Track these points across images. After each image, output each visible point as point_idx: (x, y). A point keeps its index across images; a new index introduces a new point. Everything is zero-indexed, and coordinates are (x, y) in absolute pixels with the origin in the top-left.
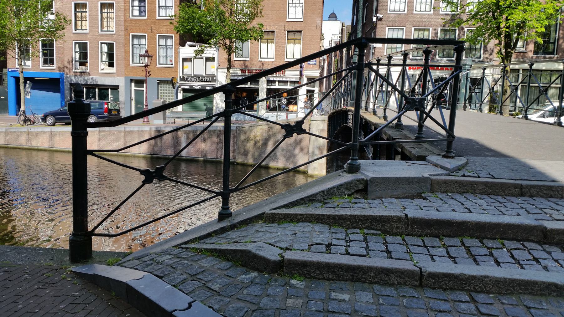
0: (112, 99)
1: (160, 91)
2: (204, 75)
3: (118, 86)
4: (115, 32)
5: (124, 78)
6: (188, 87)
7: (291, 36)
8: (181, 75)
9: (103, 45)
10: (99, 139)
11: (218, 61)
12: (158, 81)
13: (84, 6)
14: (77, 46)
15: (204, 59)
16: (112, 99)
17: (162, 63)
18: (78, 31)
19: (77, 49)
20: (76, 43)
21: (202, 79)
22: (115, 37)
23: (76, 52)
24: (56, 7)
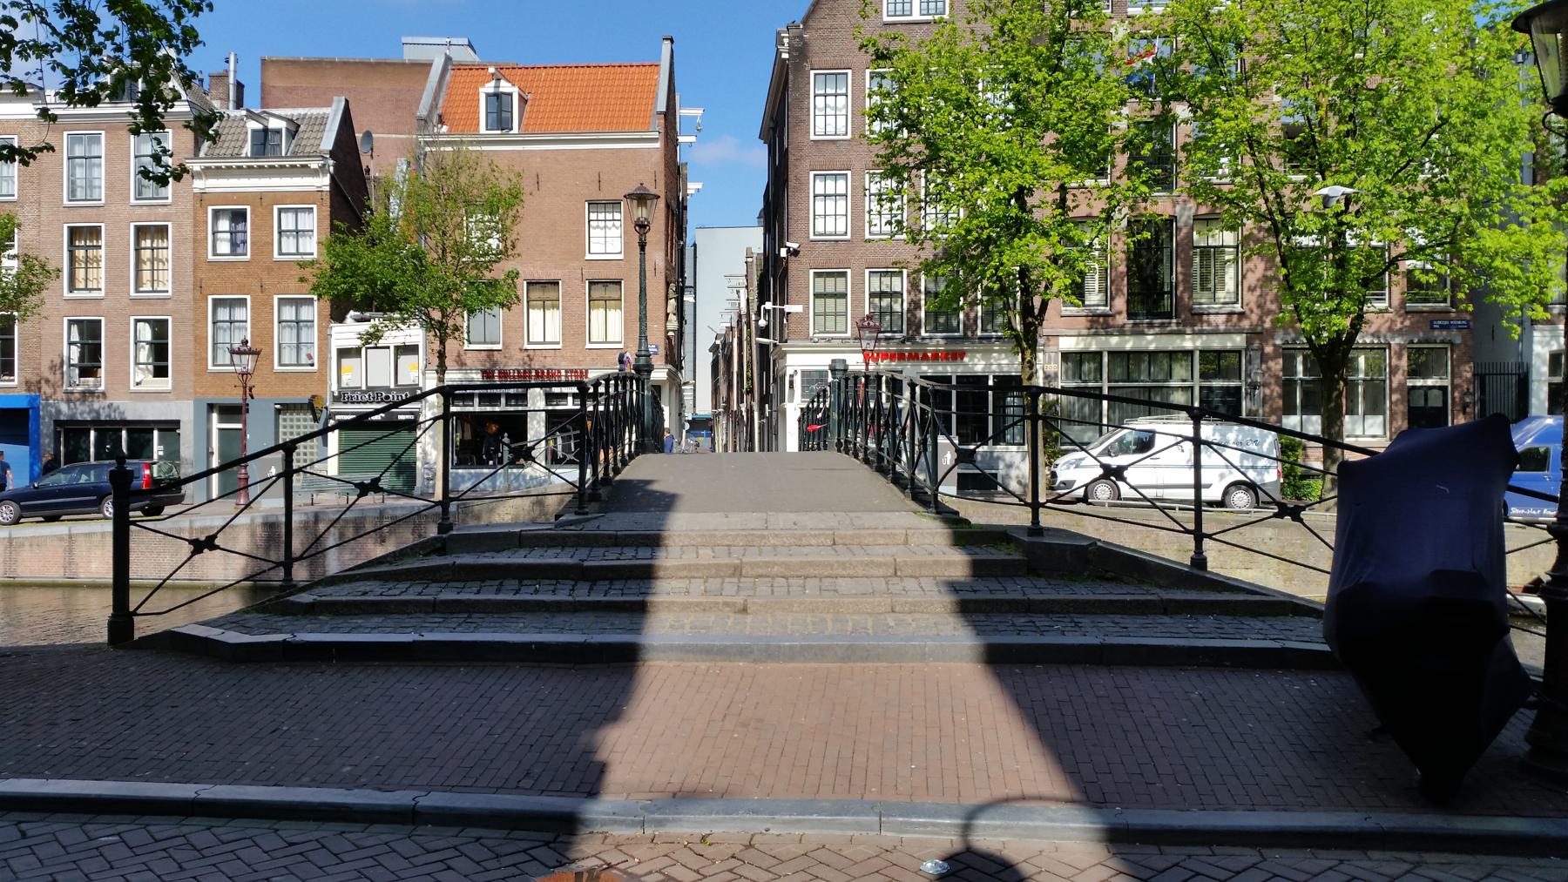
0: (161, 453)
2: (392, 386)
3: (178, 422)
7: (598, 292)
8: (334, 388)
12: (278, 406)
14: (75, 329)
15: (392, 349)
16: (161, 453)
17: (287, 362)
18: (76, 294)
20: (71, 322)
22: (171, 305)
23: (70, 344)
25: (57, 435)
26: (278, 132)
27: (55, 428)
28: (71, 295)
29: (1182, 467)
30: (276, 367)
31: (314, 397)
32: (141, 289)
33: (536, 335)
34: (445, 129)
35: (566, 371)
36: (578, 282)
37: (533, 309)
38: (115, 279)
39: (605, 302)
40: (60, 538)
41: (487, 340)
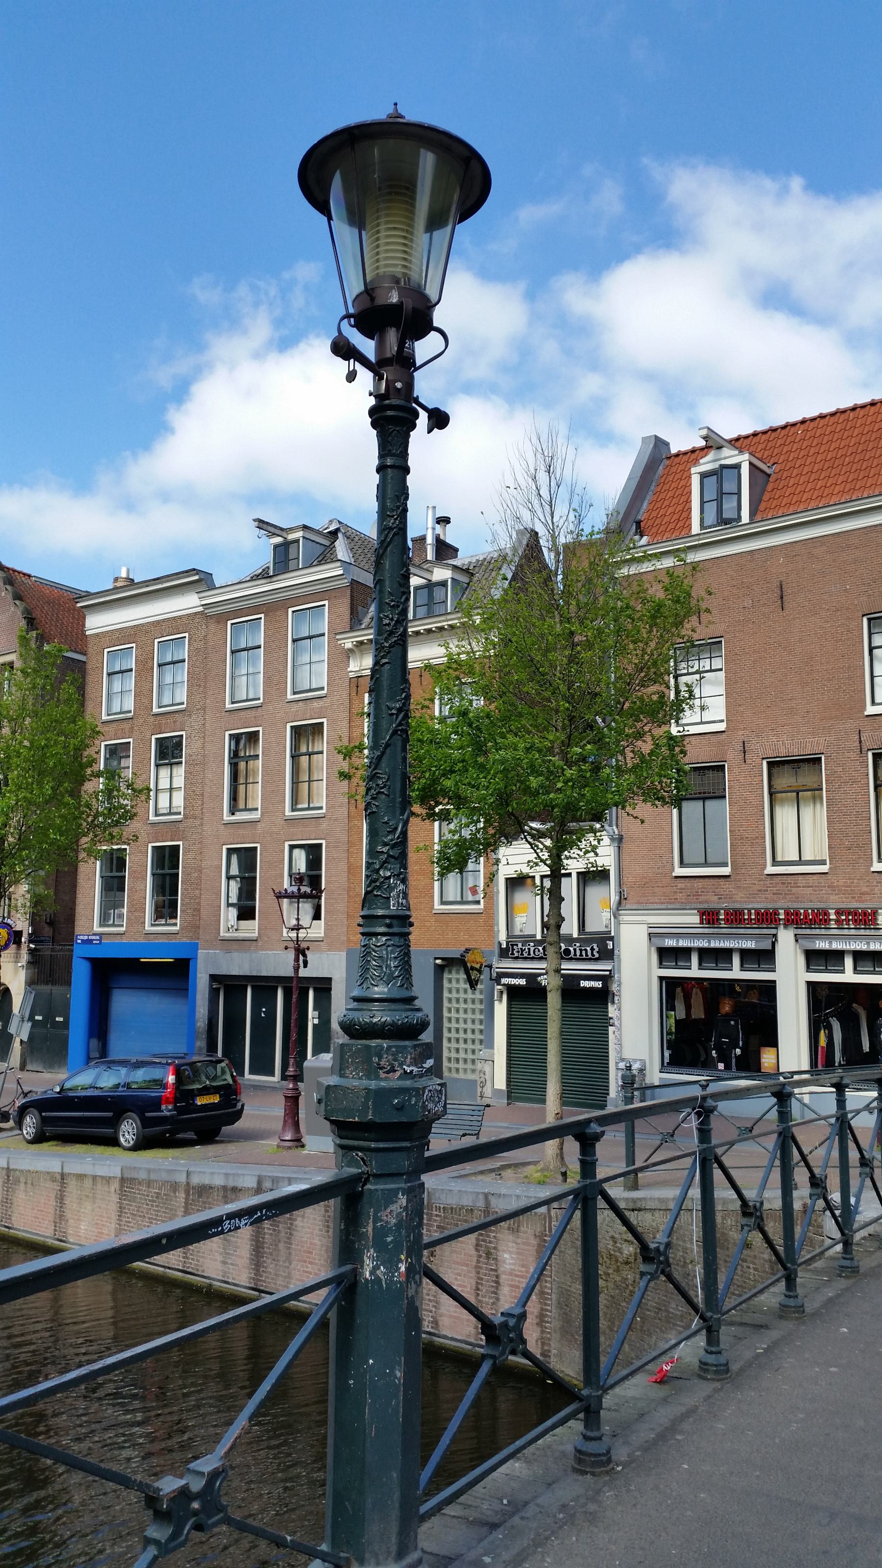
0: (316, 1021)
1: (446, 994)
2: (575, 935)
3: (330, 979)
4: (324, 811)
5: (344, 954)
6: (522, 982)
7: (785, 780)
8: (502, 937)
9: (296, 852)
10: (121, 1208)
11: (620, 884)
12: (438, 962)
13: (317, 728)
14: (234, 859)
15: (574, 876)
16: (316, 1021)
17: (451, 899)
18: (240, 816)
19: (235, 871)
20: (230, 851)
21: (567, 952)
22: (324, 825)
23: (229, 878)
24: (189, 751)
25: (214, 994)
26: (443, 584)
27: (211, 986)
28: (233, 818)
29: (431, 238)
30: (437, 906)
31: (467, 951)
32: (299, 806)
33: (788, 850)
34: (645, 540)
35: (838, 912)
36: (853, 755)
37: (782, 805)
38: (272, 795)
39: (798, 796)
40: (51, 1176)
41: (709, 860)
